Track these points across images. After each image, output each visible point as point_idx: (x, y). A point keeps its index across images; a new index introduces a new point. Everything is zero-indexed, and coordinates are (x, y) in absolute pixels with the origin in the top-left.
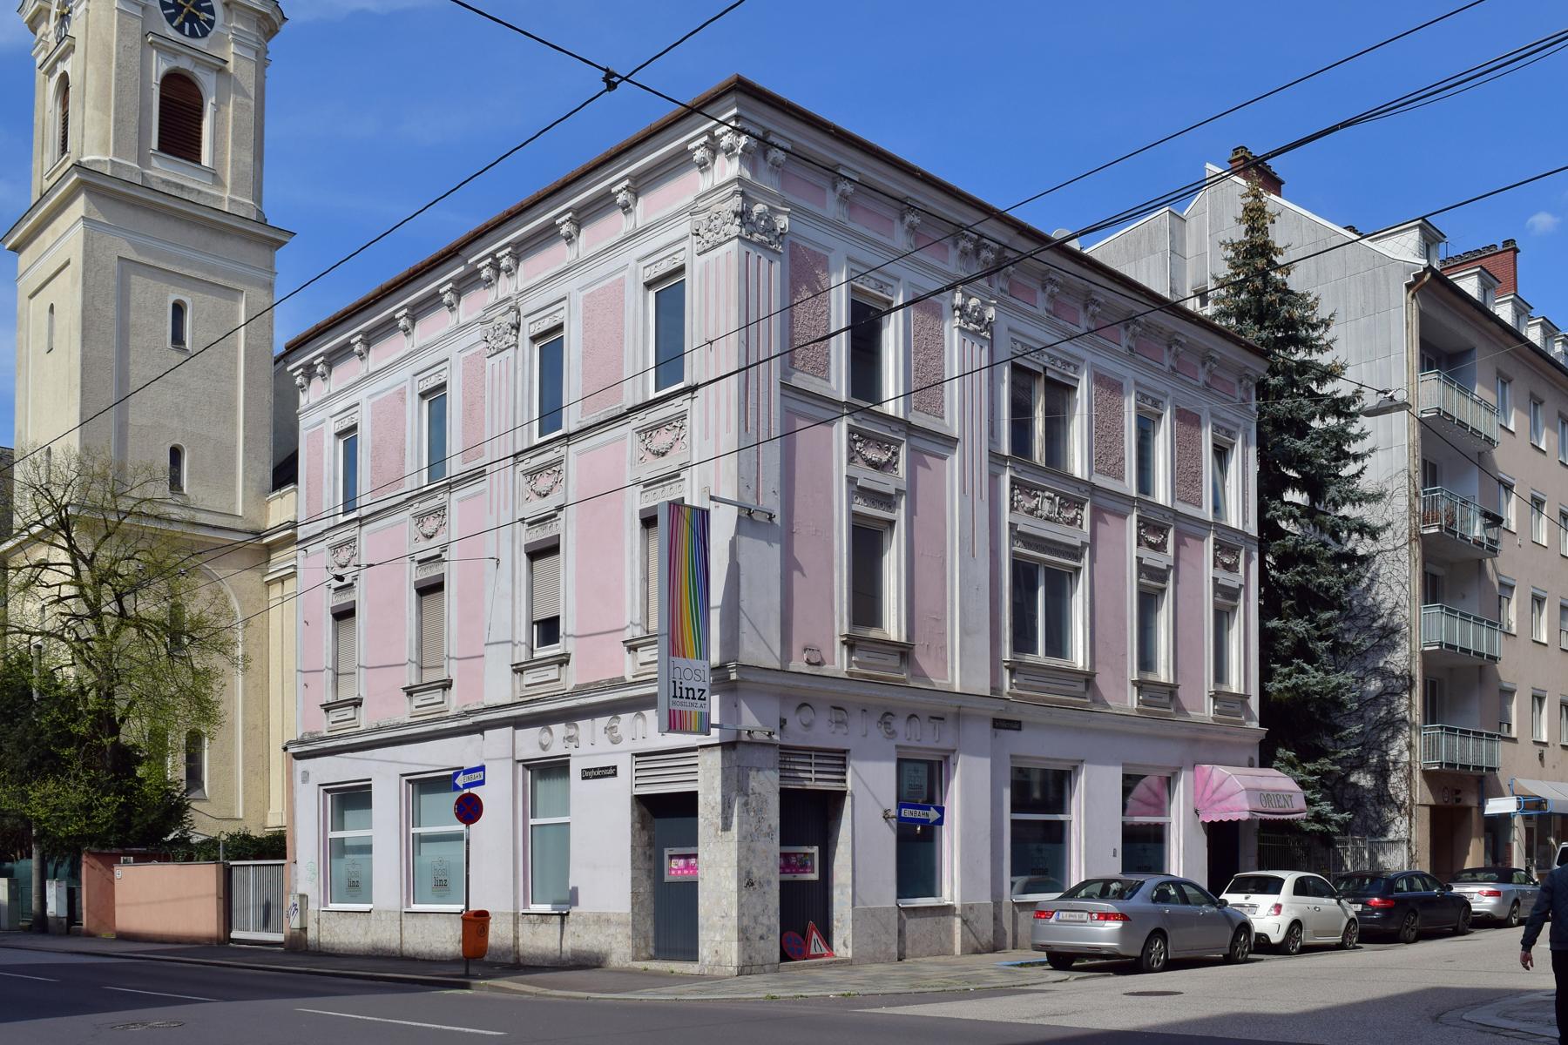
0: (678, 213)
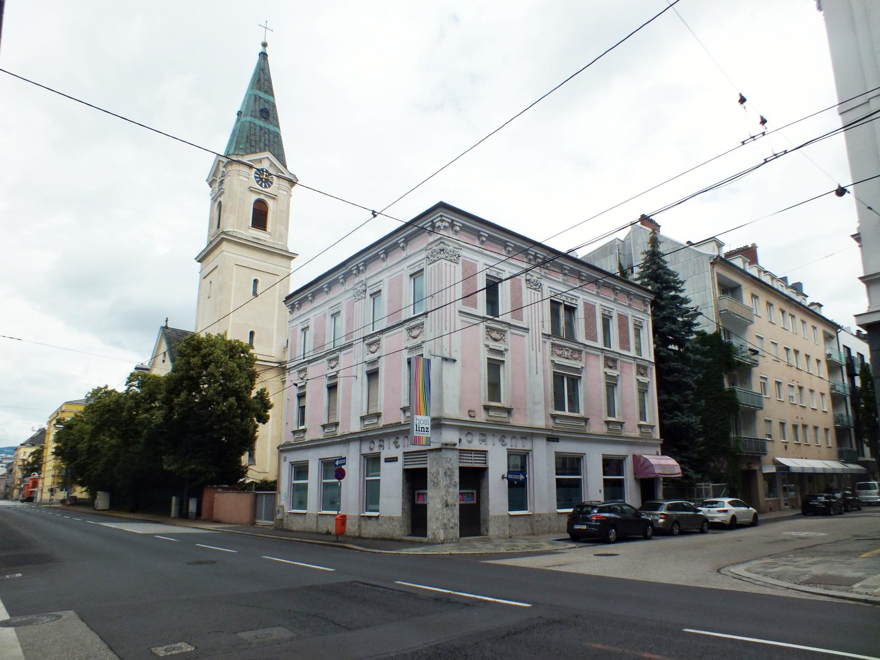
0: (422, 250)
